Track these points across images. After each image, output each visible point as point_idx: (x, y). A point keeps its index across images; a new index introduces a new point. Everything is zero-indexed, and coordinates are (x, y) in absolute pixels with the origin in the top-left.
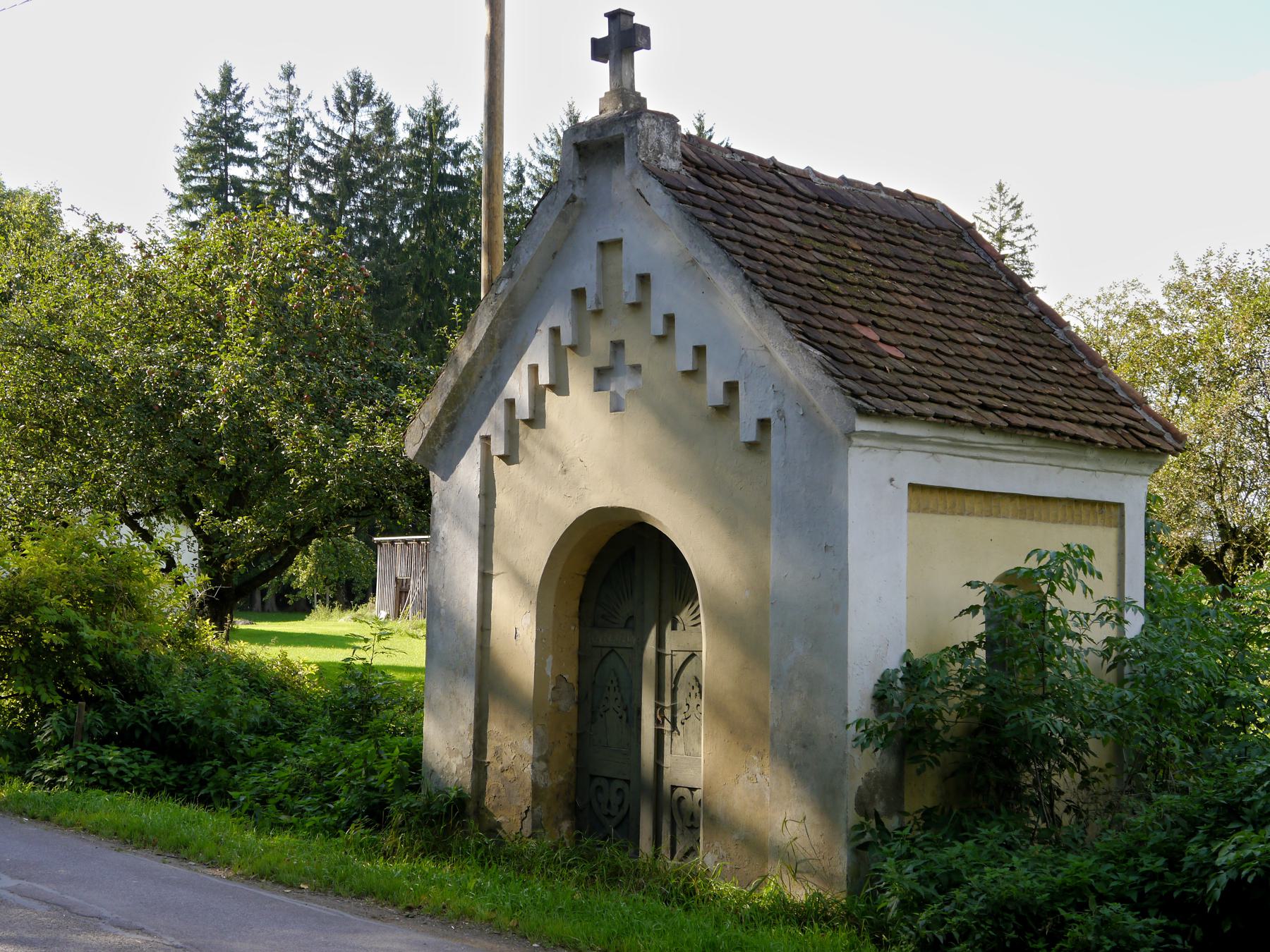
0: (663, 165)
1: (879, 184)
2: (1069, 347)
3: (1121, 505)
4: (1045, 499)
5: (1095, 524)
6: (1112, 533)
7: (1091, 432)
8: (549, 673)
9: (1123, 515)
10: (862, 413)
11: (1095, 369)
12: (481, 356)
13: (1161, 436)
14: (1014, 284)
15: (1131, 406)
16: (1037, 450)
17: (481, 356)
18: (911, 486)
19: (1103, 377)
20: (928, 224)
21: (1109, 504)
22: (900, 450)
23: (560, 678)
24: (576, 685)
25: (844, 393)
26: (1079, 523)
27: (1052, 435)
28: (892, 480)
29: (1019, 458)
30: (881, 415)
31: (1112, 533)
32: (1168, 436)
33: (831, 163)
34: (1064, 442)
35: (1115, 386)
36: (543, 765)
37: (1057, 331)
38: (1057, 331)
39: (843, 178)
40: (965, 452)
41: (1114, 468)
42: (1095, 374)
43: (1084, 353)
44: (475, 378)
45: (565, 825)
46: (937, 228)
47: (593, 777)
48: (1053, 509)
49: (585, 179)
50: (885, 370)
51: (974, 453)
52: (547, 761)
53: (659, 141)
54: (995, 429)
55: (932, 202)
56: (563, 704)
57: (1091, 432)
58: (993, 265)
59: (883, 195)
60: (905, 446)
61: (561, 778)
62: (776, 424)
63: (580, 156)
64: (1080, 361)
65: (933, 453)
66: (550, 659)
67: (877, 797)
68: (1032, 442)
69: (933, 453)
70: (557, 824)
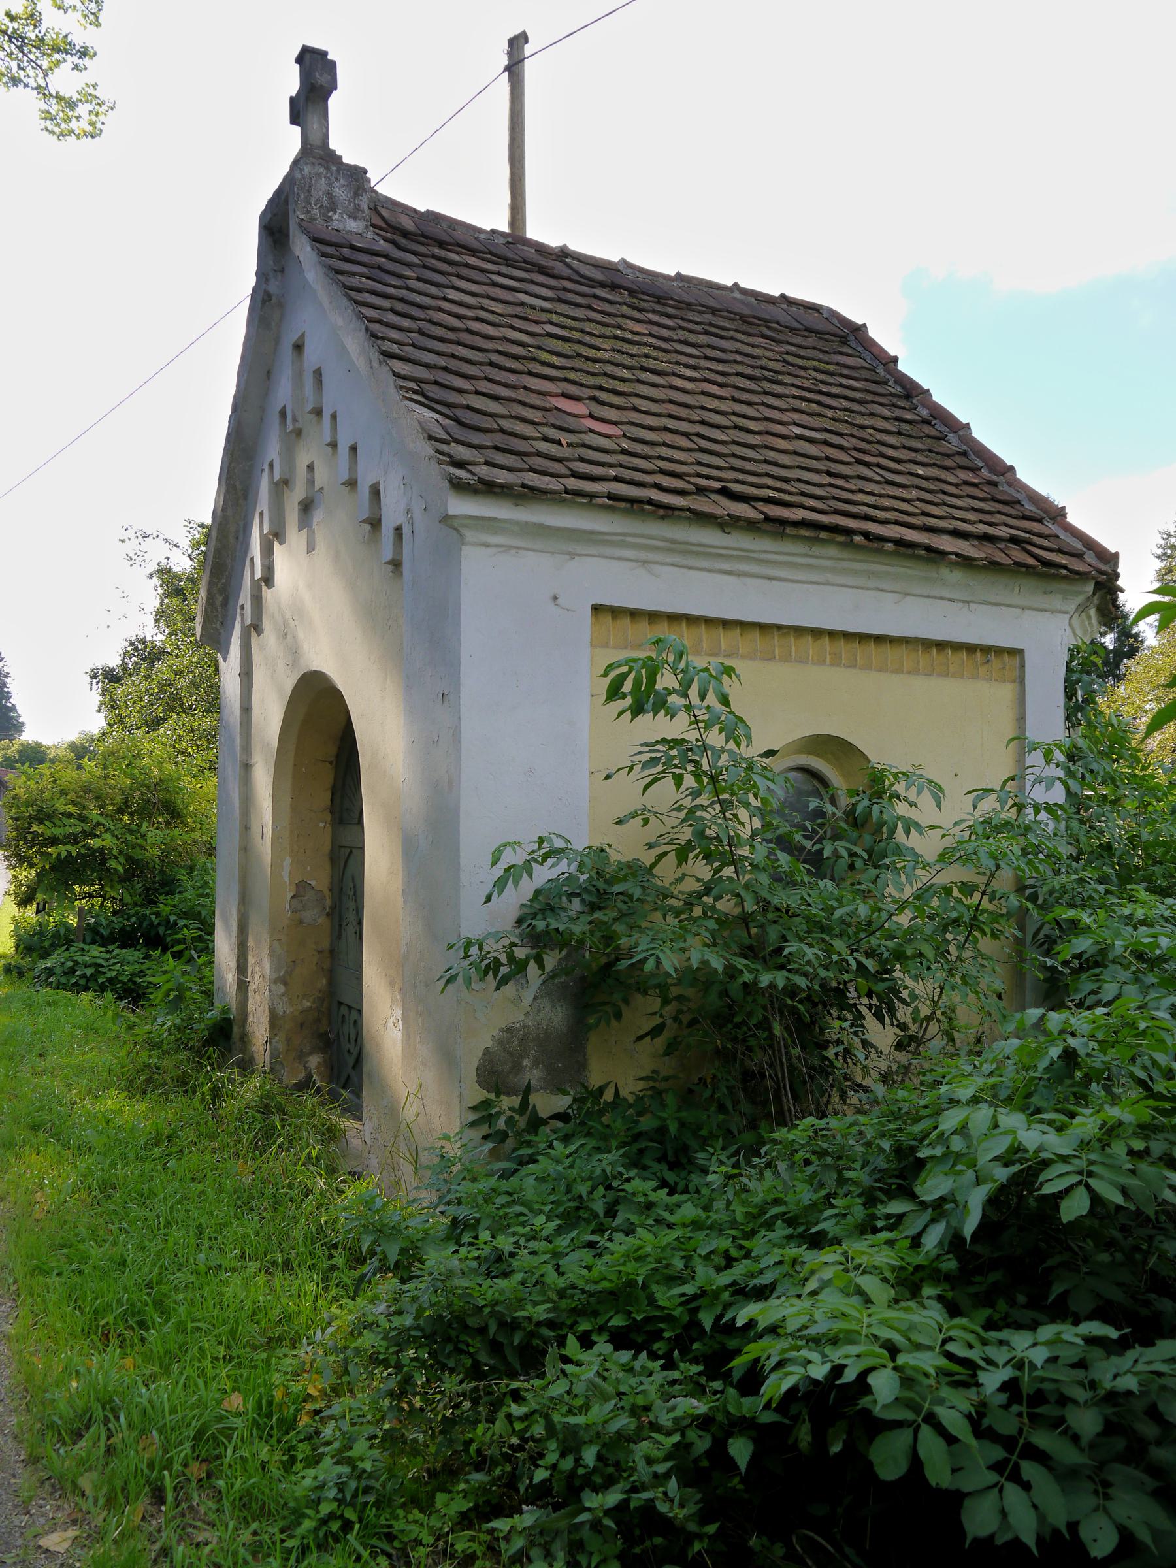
0: (336, 225)
1: (736, 284)
2: (965, 454)
3: (1019, 652)
4: (879, 639)
5: (975, 677)
6: (1006, 691)
7: (946, 543)
8: (287, 880)
9: (1023, 666)
10: (458, 486)
11: (995, 478)
12: (229, 512)
13: (1079, 556)
14: (903, 387)
15: (1040, 521)
16: (845, 564)
17: (229, 512)
18: (596, 608)
19: (1006, 488)
20: (796, 325)
21: (999, 651)
22: (573, 555)
23: (301, 887)
24: (327, 893)
25: (440, 462)
26: (946, 674)
27: (857, 539)
28: (555, 598)
29: (814, 577)
30: (488, 489)
31: (1006, 691)
32: (1090, 557)
33: (661, 256)
34: (880, 551)
35: (1019, 496)
36: (281, 988)
37: (950, 436)
38: (950, 436)
39: (678, 274)
40: (704, 563)
41: (999, 599)
42: (995, 484)
43: (983, 460)
44: (232, 540)
45: (314, 1061)
46: (807, 330)
47: (340, 1003)
48: (890, 653)
49: (282, 271)
50: (559, 443)
51: (726, 566)
52: (285, 984)
53: (330, 195)
54: (750, 526)
55: (834, 314)
56: (309, 915)
57: (946, 543)
58: (881, 370)
59: (737, 295)
60: (580, 549)
61: (307, 1004)
62: (406, 530)
63: (275, 242)
64: (975, 470)
65: (644, 562)
66: (288, 861)
67: (526, 1062)
68: (832, 551)
69: (644, 562)
70: (301, 1057)
